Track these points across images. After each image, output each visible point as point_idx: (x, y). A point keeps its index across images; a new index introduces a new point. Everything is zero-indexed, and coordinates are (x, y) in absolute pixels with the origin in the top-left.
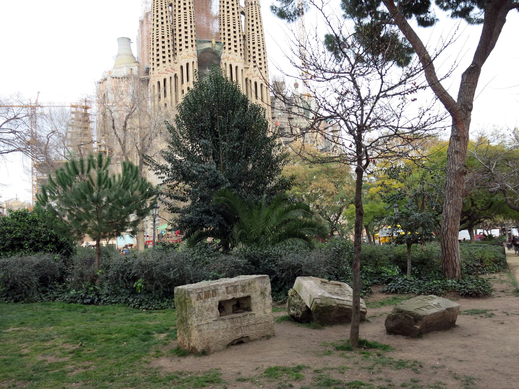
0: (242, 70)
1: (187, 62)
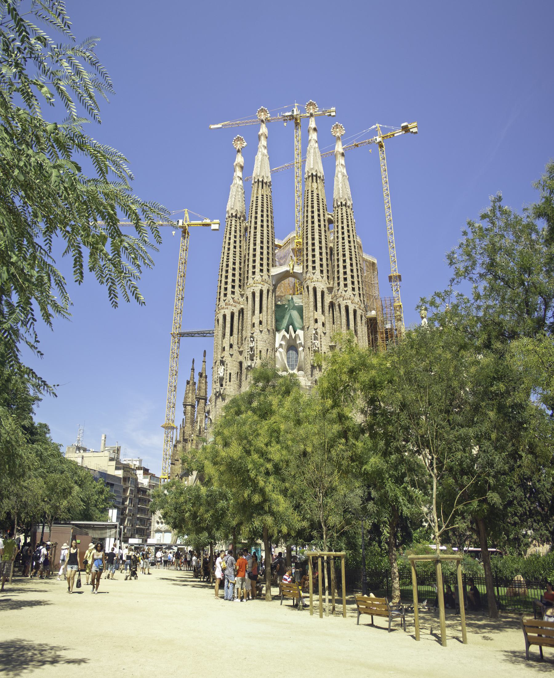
1: (252, 291)
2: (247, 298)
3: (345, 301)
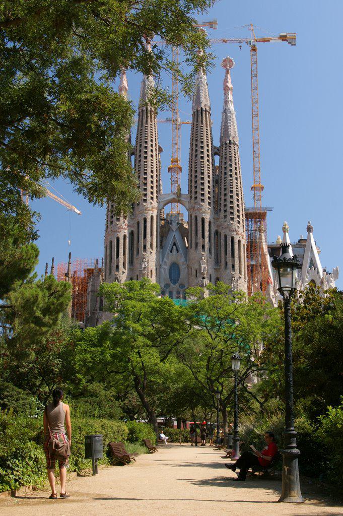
0: (210, 222)
1: (143, 217)
2: (138, 223)
3: (230, 233)
